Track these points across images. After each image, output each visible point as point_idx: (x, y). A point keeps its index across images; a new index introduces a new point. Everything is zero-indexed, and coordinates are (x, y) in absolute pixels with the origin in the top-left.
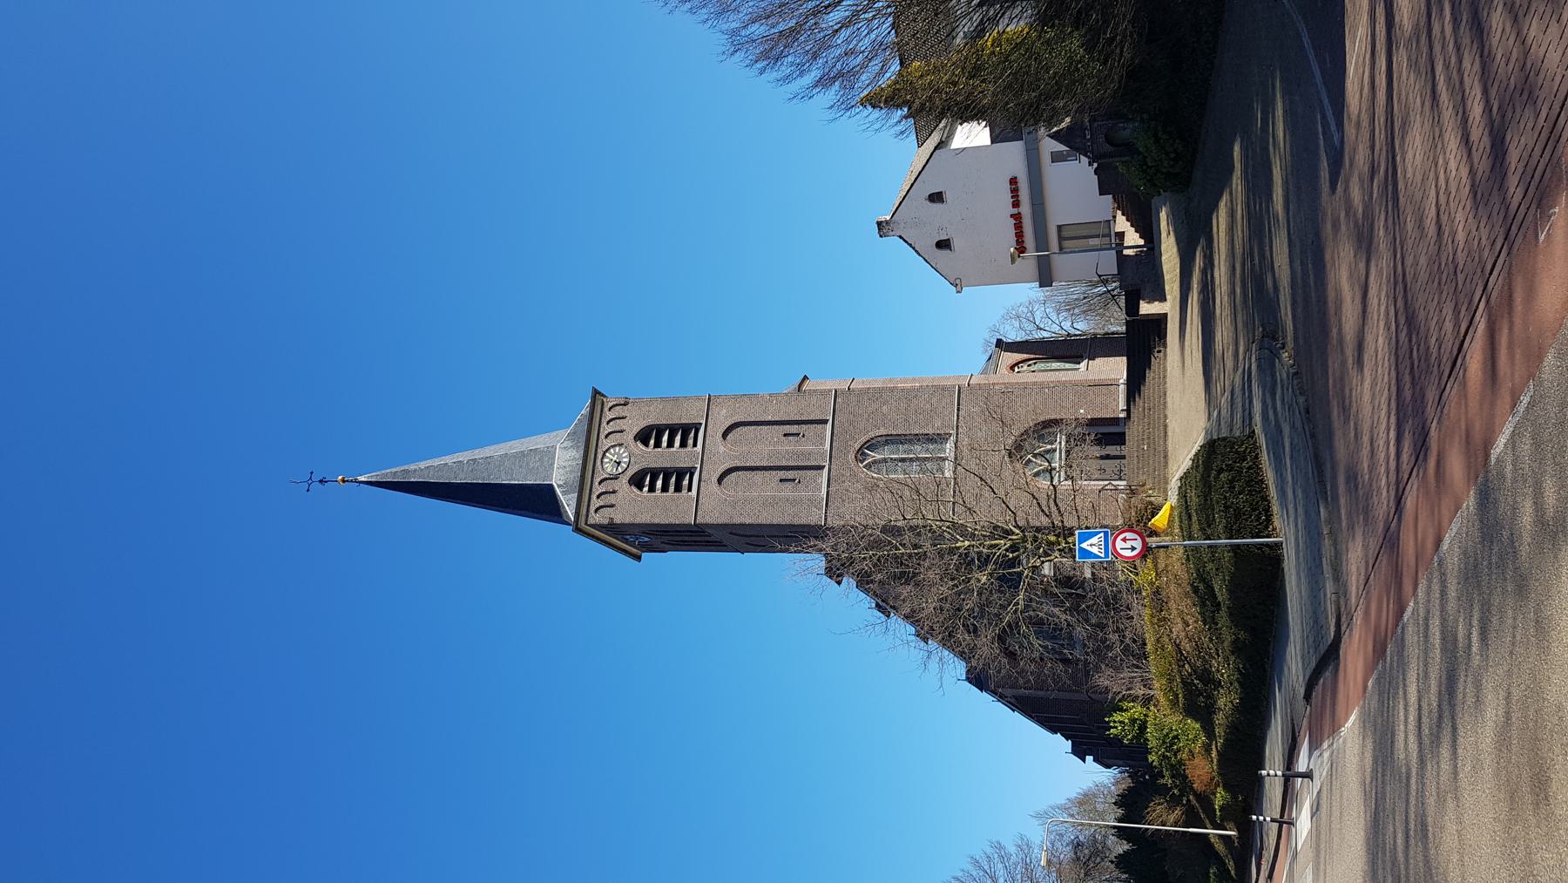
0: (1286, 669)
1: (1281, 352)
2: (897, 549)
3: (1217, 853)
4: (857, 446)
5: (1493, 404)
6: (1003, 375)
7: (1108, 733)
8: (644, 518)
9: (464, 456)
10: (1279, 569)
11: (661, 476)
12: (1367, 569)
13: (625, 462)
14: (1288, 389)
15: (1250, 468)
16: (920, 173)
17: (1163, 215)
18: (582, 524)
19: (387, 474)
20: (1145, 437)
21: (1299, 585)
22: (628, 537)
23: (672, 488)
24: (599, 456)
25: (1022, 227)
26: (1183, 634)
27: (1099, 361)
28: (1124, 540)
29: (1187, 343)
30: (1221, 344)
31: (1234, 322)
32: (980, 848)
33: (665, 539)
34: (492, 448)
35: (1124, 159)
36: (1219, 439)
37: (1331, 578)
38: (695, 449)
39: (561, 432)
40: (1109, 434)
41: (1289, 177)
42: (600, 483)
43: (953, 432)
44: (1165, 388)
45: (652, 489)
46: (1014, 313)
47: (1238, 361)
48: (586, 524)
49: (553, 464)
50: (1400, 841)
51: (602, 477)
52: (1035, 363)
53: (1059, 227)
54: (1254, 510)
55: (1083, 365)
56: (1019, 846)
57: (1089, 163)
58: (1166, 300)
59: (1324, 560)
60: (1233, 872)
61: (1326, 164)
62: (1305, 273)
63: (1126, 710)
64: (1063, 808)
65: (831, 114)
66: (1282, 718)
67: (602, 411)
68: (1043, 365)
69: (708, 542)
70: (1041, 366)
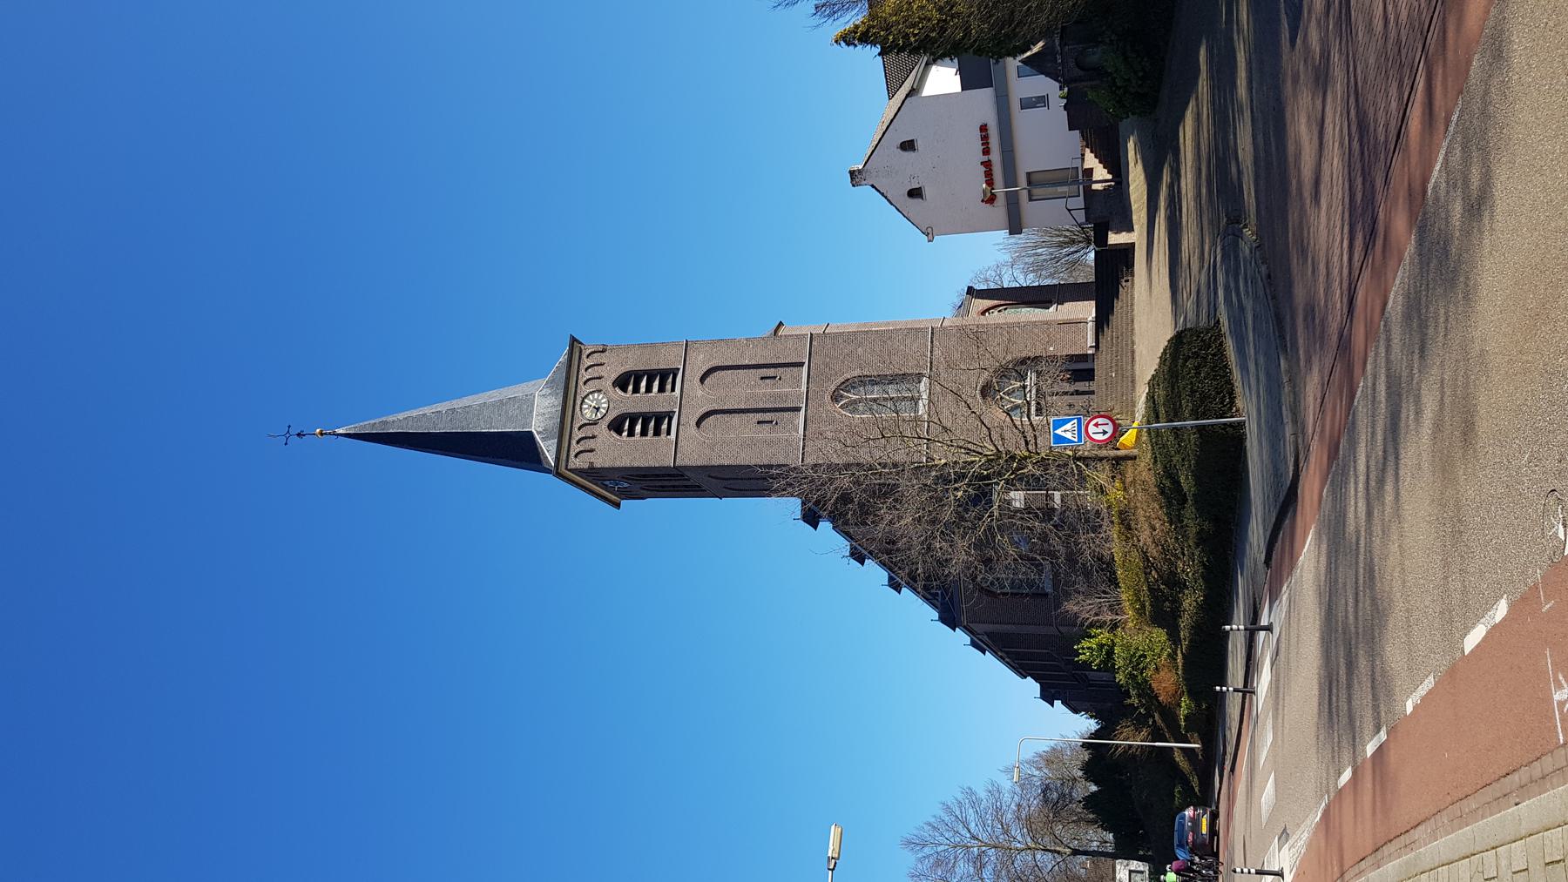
0: (1248, 547)
1: (1244, 230)
3: (1182, 771)
4: (833, 388)
5: (1431, 134)
6: (973, 318)
7: (1076, 659)
8: (625, 462)
9: (443, 407)
10: (1241, 449)
11: (640, 421)
12: (1323, 388)
13: (604, 408)
14: (1251, 263)
15: (1214, 355)
16: (892, 121)
17: (1131, 145)
18: (562, 469)
21: (1260, 455)
22: (607, 483)
23: (651, 432)
24: (578, 402)
26: (1151, 540)
30: (1187, 251)
31: (1200, 225)
33: (644, 484)
35: (1094, 83)
36: (1185, 330)
37: (1290, 423)
38: (673, 393)
40: (1080, 370)
41: (1253, 56)
42: (579, 429)
46: (982, 277)
47: (1203, 260)
48: (566, 469)
49: (532, 412)
50: (1351, 618)
51: (582, 423)
52: (1005, 309)
53: (1029, 174)
54: (1218, 393)
55: (1052, 309)
56: (990, 792)
57: (1060, 87)
59: (1284, 408)
60: (1197, 790)
61: (1286, 26)
62: (1267, 143)
63: (1094, 637)
65: (817, 20)
66: (1244, 602)
67: (580, 358)
69: (686, 486)
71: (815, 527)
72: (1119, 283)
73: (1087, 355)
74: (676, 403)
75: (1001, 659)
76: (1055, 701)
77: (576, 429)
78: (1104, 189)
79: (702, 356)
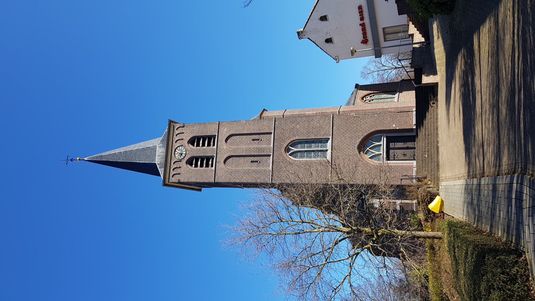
4: (285, 145)
13: (184, 154)
17: (435, 26)
19: (95, 156)
20: (426, 150)
24: (173, 151)
25: (365, 30)
27: (404, 93)
29: (451, 111)
34: (133, 145)
38: (214, 147)
39: (158, 139)
42: (174, 164)
43: (331, 137)
44: (437, 126)
45: (196, 166)
48: (169, 182)
49: (155, 154)
51: (175, 161)
52: (373, 95)
53: (384, 29)
55: (397, 95)
58: (437, 74)
68: (377, 96)
70: (376, 96)
72: (429, 104)
73: (413, 129)
74: (215, 152)
77: (172, 164)
78: (420, 47)
79: (226, 129)
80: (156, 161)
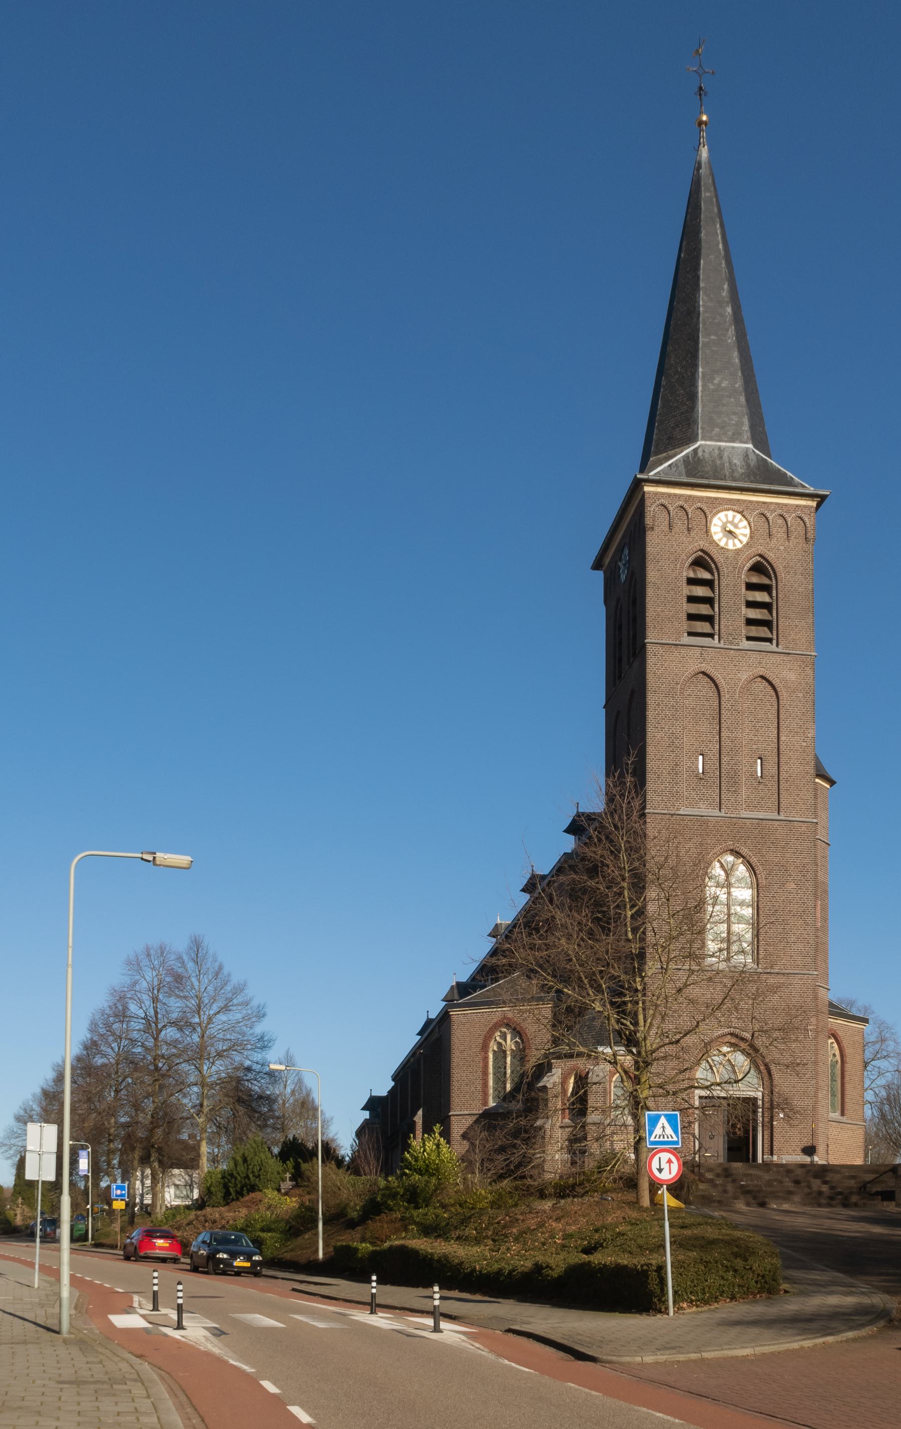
2: (632, 907)
22: (626, 552)
28: (670, 1161)
32: (257, 994)
56: (262, 1037)
64: (300, 1082)
69: (620, 660)
71: (568, 831)
74: (731, 643)
75: (413, 1054)
76: (368, 1112)
80: (703, 442)
